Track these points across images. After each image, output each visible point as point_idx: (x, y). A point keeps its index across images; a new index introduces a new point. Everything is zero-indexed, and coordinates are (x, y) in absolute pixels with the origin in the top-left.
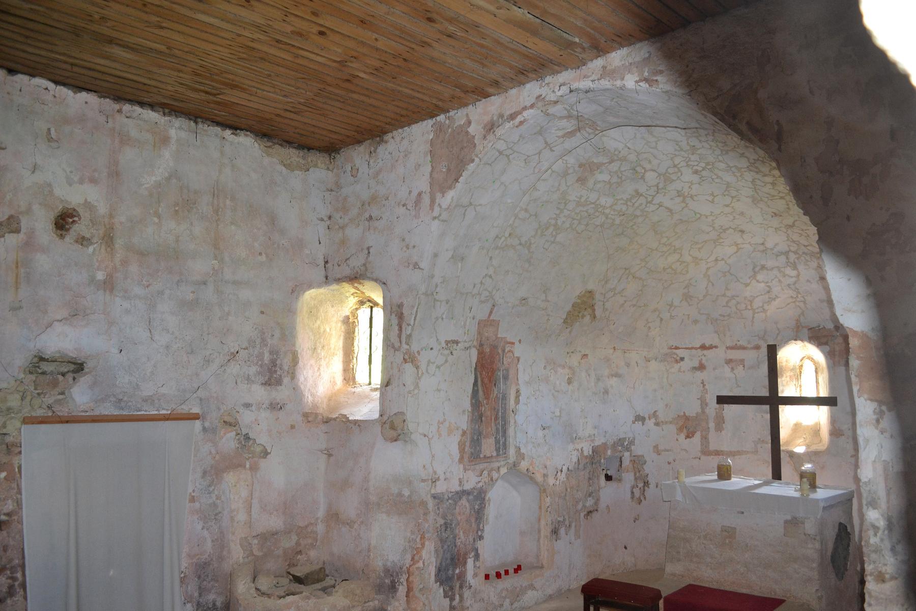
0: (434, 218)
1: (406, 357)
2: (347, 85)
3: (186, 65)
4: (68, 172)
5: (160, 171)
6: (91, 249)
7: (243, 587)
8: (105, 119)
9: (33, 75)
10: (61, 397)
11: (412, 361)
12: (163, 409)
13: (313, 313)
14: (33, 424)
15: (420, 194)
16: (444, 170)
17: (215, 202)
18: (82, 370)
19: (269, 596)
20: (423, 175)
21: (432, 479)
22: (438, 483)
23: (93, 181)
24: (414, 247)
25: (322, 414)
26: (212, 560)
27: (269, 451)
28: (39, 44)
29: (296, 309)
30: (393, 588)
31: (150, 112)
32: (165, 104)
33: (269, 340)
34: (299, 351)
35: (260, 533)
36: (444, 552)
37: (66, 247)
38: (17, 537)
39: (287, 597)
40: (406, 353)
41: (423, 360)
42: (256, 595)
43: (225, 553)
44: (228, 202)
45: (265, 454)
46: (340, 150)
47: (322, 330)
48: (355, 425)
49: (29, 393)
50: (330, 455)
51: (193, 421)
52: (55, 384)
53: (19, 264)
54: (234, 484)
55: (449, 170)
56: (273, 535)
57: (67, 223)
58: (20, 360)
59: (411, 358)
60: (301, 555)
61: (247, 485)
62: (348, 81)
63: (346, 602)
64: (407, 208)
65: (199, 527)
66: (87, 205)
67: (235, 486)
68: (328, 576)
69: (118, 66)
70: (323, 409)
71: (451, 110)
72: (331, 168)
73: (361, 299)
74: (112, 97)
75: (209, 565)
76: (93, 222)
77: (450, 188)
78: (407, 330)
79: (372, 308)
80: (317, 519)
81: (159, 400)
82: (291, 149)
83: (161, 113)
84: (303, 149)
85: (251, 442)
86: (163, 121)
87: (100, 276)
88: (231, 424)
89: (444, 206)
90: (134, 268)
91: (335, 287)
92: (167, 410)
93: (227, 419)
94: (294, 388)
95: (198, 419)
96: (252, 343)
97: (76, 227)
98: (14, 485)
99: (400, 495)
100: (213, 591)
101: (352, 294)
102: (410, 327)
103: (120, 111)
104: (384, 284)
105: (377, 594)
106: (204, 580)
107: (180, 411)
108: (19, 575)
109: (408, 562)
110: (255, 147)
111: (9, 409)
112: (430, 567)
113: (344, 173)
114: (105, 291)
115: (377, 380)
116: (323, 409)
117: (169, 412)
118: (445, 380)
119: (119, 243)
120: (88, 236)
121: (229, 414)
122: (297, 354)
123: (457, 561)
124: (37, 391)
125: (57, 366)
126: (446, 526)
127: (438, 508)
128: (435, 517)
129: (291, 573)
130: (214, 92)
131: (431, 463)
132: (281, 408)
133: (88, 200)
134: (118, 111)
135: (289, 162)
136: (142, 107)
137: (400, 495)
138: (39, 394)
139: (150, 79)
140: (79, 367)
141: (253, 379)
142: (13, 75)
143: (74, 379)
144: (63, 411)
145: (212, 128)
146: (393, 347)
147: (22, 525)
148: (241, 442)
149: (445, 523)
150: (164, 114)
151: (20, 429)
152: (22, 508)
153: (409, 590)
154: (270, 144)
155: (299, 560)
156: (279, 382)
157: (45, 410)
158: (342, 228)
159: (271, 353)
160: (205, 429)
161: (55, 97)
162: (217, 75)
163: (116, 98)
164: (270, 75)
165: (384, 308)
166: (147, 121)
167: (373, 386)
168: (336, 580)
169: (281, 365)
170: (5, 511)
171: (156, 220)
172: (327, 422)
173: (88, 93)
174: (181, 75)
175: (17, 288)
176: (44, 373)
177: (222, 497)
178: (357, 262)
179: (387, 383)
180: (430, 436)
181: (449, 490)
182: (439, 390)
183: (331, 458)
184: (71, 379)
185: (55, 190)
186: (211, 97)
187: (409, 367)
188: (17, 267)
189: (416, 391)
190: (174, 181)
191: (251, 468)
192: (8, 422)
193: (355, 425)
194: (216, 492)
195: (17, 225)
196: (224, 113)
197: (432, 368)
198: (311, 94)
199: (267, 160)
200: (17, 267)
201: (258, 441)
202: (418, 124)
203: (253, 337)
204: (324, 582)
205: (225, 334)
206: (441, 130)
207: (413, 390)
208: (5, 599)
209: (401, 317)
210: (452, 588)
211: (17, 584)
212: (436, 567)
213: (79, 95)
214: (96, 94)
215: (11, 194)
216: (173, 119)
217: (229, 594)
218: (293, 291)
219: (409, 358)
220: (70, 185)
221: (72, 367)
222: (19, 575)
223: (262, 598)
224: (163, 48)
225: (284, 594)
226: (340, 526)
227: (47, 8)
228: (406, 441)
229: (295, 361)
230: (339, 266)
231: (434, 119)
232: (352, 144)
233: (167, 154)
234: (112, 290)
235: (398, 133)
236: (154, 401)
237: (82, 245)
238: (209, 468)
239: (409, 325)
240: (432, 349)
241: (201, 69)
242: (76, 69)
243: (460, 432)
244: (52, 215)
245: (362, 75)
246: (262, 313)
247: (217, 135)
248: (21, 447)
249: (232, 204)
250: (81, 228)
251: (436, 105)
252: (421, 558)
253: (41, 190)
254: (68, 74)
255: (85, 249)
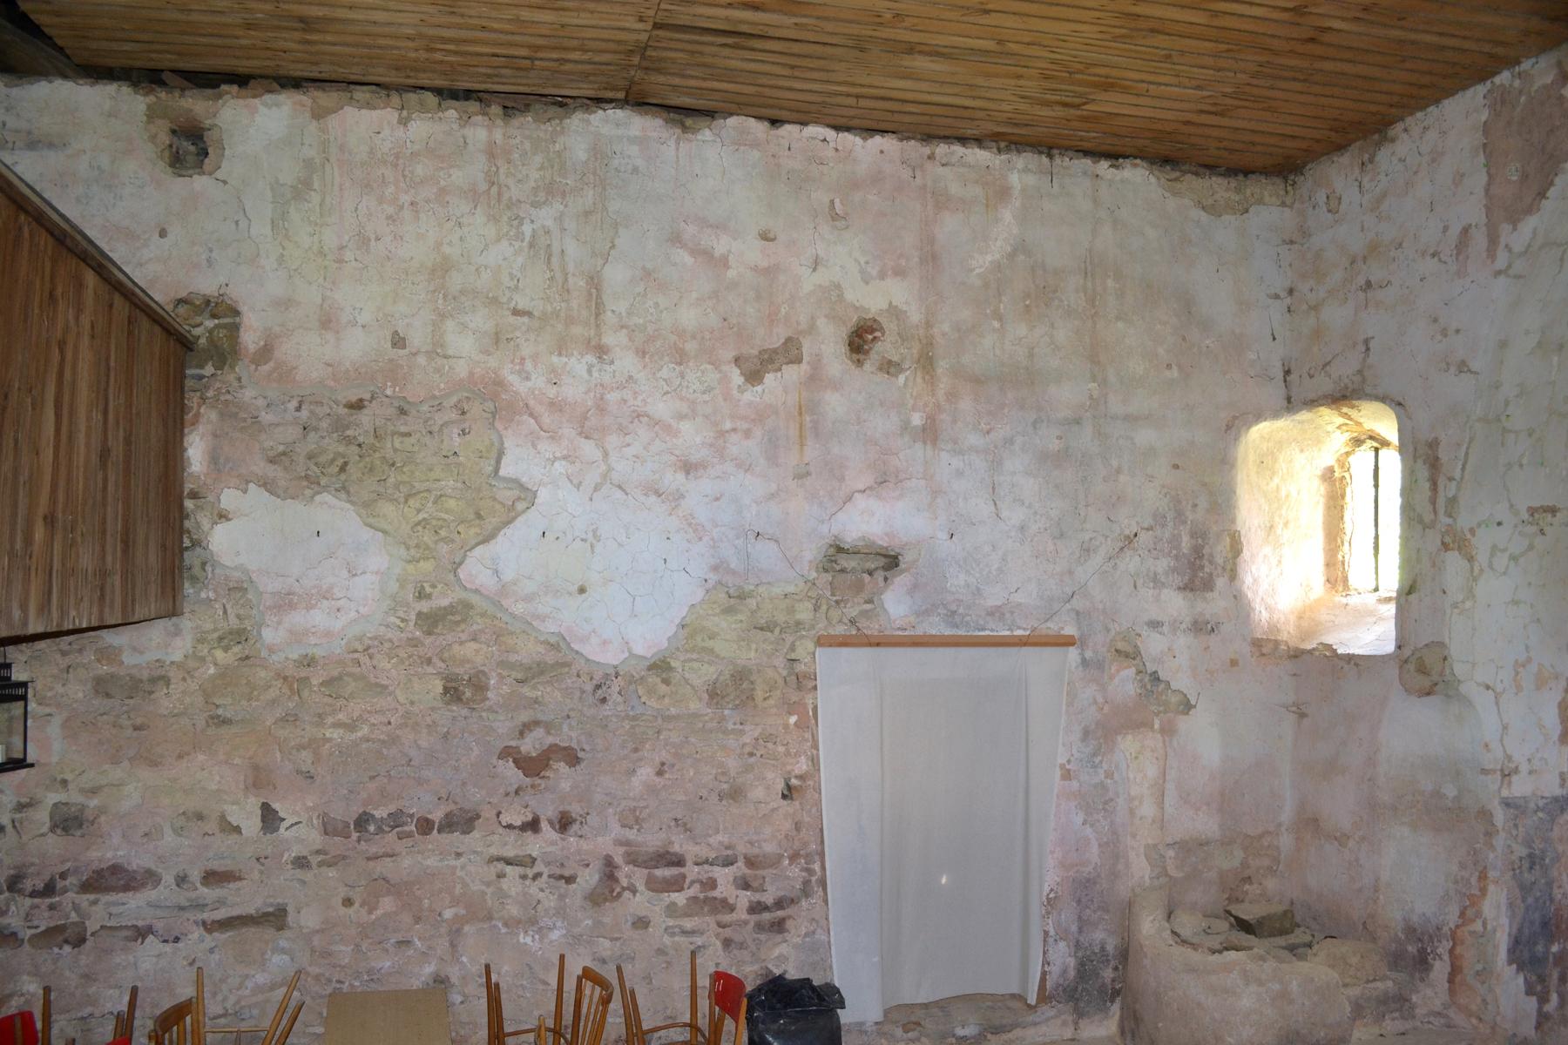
0: (1498, 273)
1: (1448, 539)
2: (1311, 48)
3: (1030, 64)
4: (862, 262)
5: (999, 243)
6: (902, 379)
7: (1149, 926)
8: (911, 173)
9: (804, 124)
10: (868, 607)
11: (1459, 547)
12: (1019, 628)
13: (1266, 463)
14: (831, 646)
15: (1466, 231)
16: (1515, 178)
17: (1089, 284)
18: (897, 565)
19: (1194, 947)
20: (1471, 193)
21: (1502, 770)
22: (1514, 778)
23: (900, 273)
24: (1458, 331)
25: (1286, 642)
26: (1099, 876)
27: (1193, 702)
28: (808, 75)
29: (1236, 459)
30: (1422, 963)
31: (977, 150)
32: (999, 134)
33: (1188, 513)
34: (1243, 533)
35: (1178, 840)
36: (1527, 909)
37: (867, 378)
38: (814, 810)
39: (1225, 953)
40: (1447, 532)
41: (1482, 544)
42: (1171, 942)
43: (1120, 867)
44: (1110, 283)
45: (1187, 707)
46: (1304, 167)
47: (1283, 493)
48: (1349, 663)
49: (824, 601)
50: (1303, 715)
51: (1065, 648)
52: (859, 587)
54: (1133, 755)
55: (1525, 177)
56: (1201, 845)
57: (865, 342)
58: (811, 552)
59: (1455, 542)
60: (1251, 883)
61: (1157, 759)
62: (1312, 40)
63: (1334, 975)
64: (1440, 260)
65: (1079, 819)
66: (894, 312)
67: (1136, 758)
68: (1299, 926)
69: (924, 86)
70: (1288, 634)
71: (1524, 60)
72: (1288, 203)
73: (1356, 434)
74: (919, 137)
75: (1095, 883)
76: (903, 337)
77: (1529, 211)
78: (1447, 490)
79: (1377, 450)
80: (1280, 825)
81: (1012, 613)
82: (1214, 179)
83: (995, 150)
84: (1236, 175)
85: (1162, 686)
86: (997, 162)
87: (917, 420)
88: (1130, 655)
89: (1517, 248)
90: (966, 404)
91: (1304, 415)
92: (1024, 629)
93: (1120, 645)
94: (1235, 597)
95: (1073, 644)
96: (1159, 519)
97: (878, 346)
98: (808, 735)
99: (1437, 794)
100: (1100, 927)
101: (1339, 427)
102: (1454, 483)
103: (931, 157)
104: (1400, 404)
105: (1390, 970)
106: (1087, 907)
107: (1044, 632)
108: (817, 867)
109: (1452, 917)
110: (1150, 184)
111: (798, 623)
112: (1498, 934)
113: (1314, 207)
114: (925, 443)
115: (1391, 581)
116: (1289, 633)
117: (1028, 633)
118: (1530, 584)
119: (942, 366)
120: (895, 359)
121: (1124, 639)
122: (1239, 536)
123: (1554, 929)
124: (835, 598)
125: (861, 559)
126: (1533, 860)
127: (1516, 826)
128: (1509, 842)
129: (1233, 912)
130: (1077, 101)
131: (1501, 740)
132: (1213, 630)
133: (894, 304)
134: (929, 158)
135: (1210, 201)
136: (964, 145)
137: (1437, 794)
138: (837, 602)
139: (974, 98)
140: (891, 562)
141: (1163, 580)
142: (777, 128)
143: (886, 579)
144: (871, 628)
145: (1076, 162)
146: (1421, 521)
147: (820, 794)
148: (1145, 686)
149: (1531, 856)
150: (999, 151)
151: (814, 654)
152: (819, 770)
153: (1455, 971)
154: (1177, 174)
155: (1247, 893)
156: (1208, 585)
157: (846, 624)
158: (1315, 308)
159: (1193, 535)
160: (1085, 662)
161: (837, 150)
162: (1080, 72)
163: (925, 137)
164: (1169, 56)
165: (1402, 449)
166: (973, 166)
167: (1383, 593)
168: (1313, 936)
169: (1211, 555)
170: (797, 772)
171: (996, 324)
172: (1296, 657)
174: (1021, 82)
175: (802, 445)
176: (843, 571)
177: (1115, 775)
178: (1345, 369)
179: (1408, 590)
180: (1499, 688)
181: (1539, 794)
182: (1516, 603)
183: (1305, 720)
184: (881, 580)
186: (1072, 111)
187: (1454, 560)
188: (800, 414)
189: (1468, 604)
190: (1022, 257)
191: (1163, 731)
192: (798, 643)
193: (1349, 663)
194: (1105, 766)
196: (1095, 134)
197: (1502, 561)
198: (1244, 76)
199: (1172, 203)
201: (1174, 686)
202: (1457, 97)
203: (1161, 510)
204: (1292, 936)
205: (1113, 505)
206: (1503, 102)
207: (1463, 602)
208: (799, 900)
209: (1434, 464)
210: (1542, 979)
211: (814, 879)
212: (1509, 935)
213: (870, 141)
214: (894, 136)
215: (786, 306)
216: (1014, 157)
217: (1126, 934)
218: (1229, 428)
219: (1454, 542)
220: (867, 283)
221: (882, 561)
222: (817, 867)
223: (1183, 949)
224: (990, 45)
225: (1218, 947)
226: (1323, 842)
227: (818, 18)
228: (1447, 696)
229: (1236, 549)
230: (1311, 377)
231: (1488, 83)
232: (1327, 154)
233: (1007, 215)
234: (935, 441)
235: (1415, 121)
236: (1004, 614)
237: (888, 373)
238: (1093, 727)
239: (1451, 479)
240: (1499, 524)
241: (1054, 67)
242: (862, 103)
244: (844, 333)
245: (1336, 24)
246: (1176, 467)
247: (1085, 173)
249: (1117, 286)
250: (885, 347)
251: (1491, 56)
252: (1479, 914)
253: (826, 295)
254: (852, 112)
255: (893, 379)
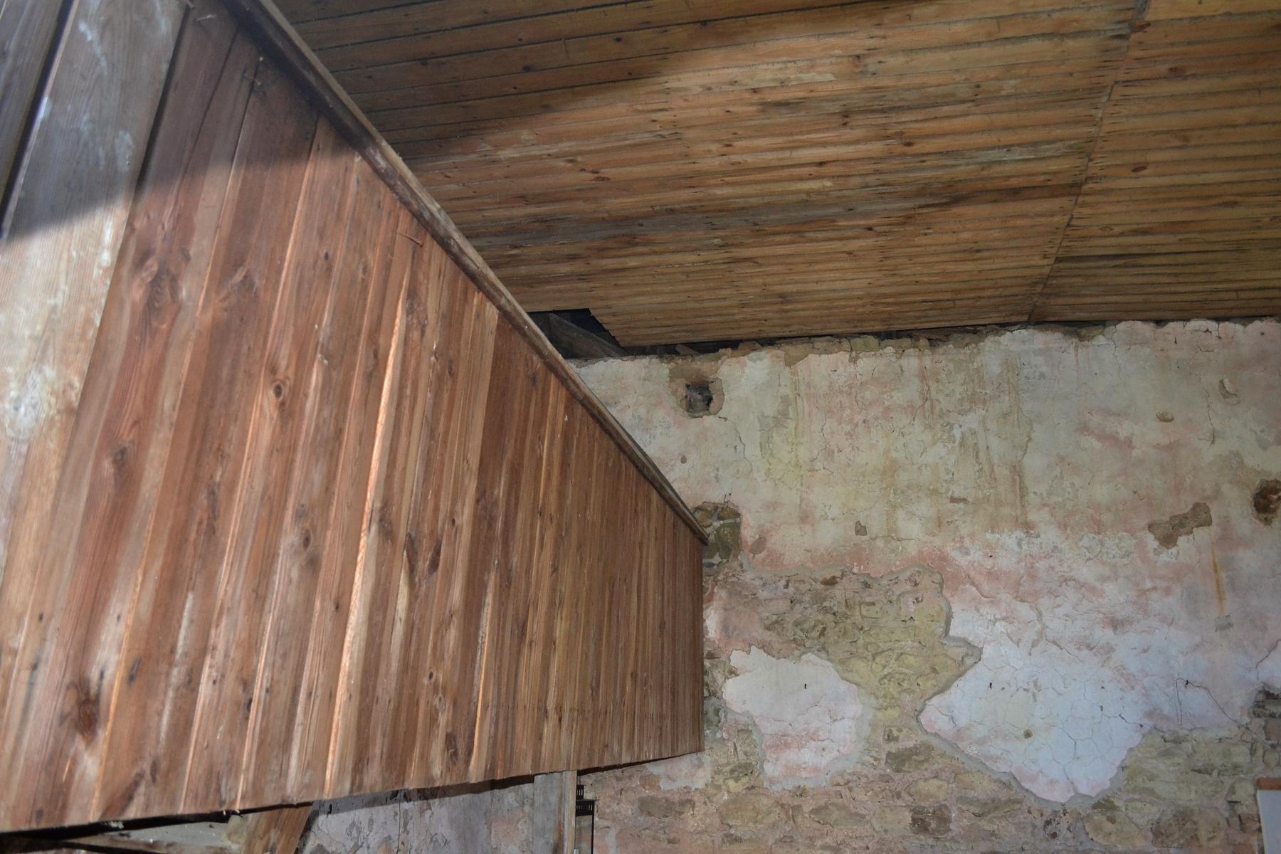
53: (1218, 567)
57: (1271, 502)
111: (1235, 767)
124: (1270, 742)
138: (1273, 746)
151: (1255, 796)
161: (1220, 338)
173: (1262, 321)
185: (1246, 460)
188: (1216, 571)
192: (1237, 786)
195: (1205, 515)
200: (1216, 571)
214: (1272, 319)
242: (1243, 295)
243: (1014, 601)
244: (1248, 495)
248: (1260, 822)
254: (1230, 304)
